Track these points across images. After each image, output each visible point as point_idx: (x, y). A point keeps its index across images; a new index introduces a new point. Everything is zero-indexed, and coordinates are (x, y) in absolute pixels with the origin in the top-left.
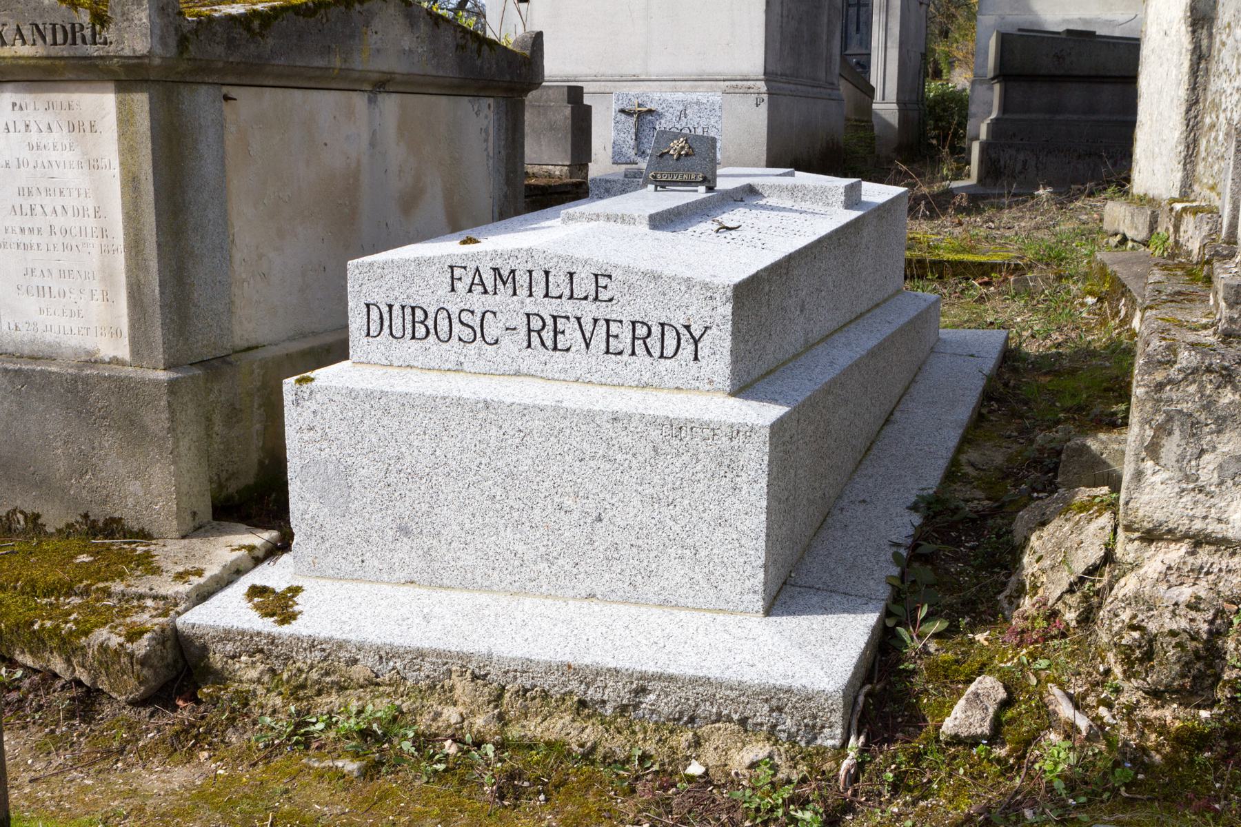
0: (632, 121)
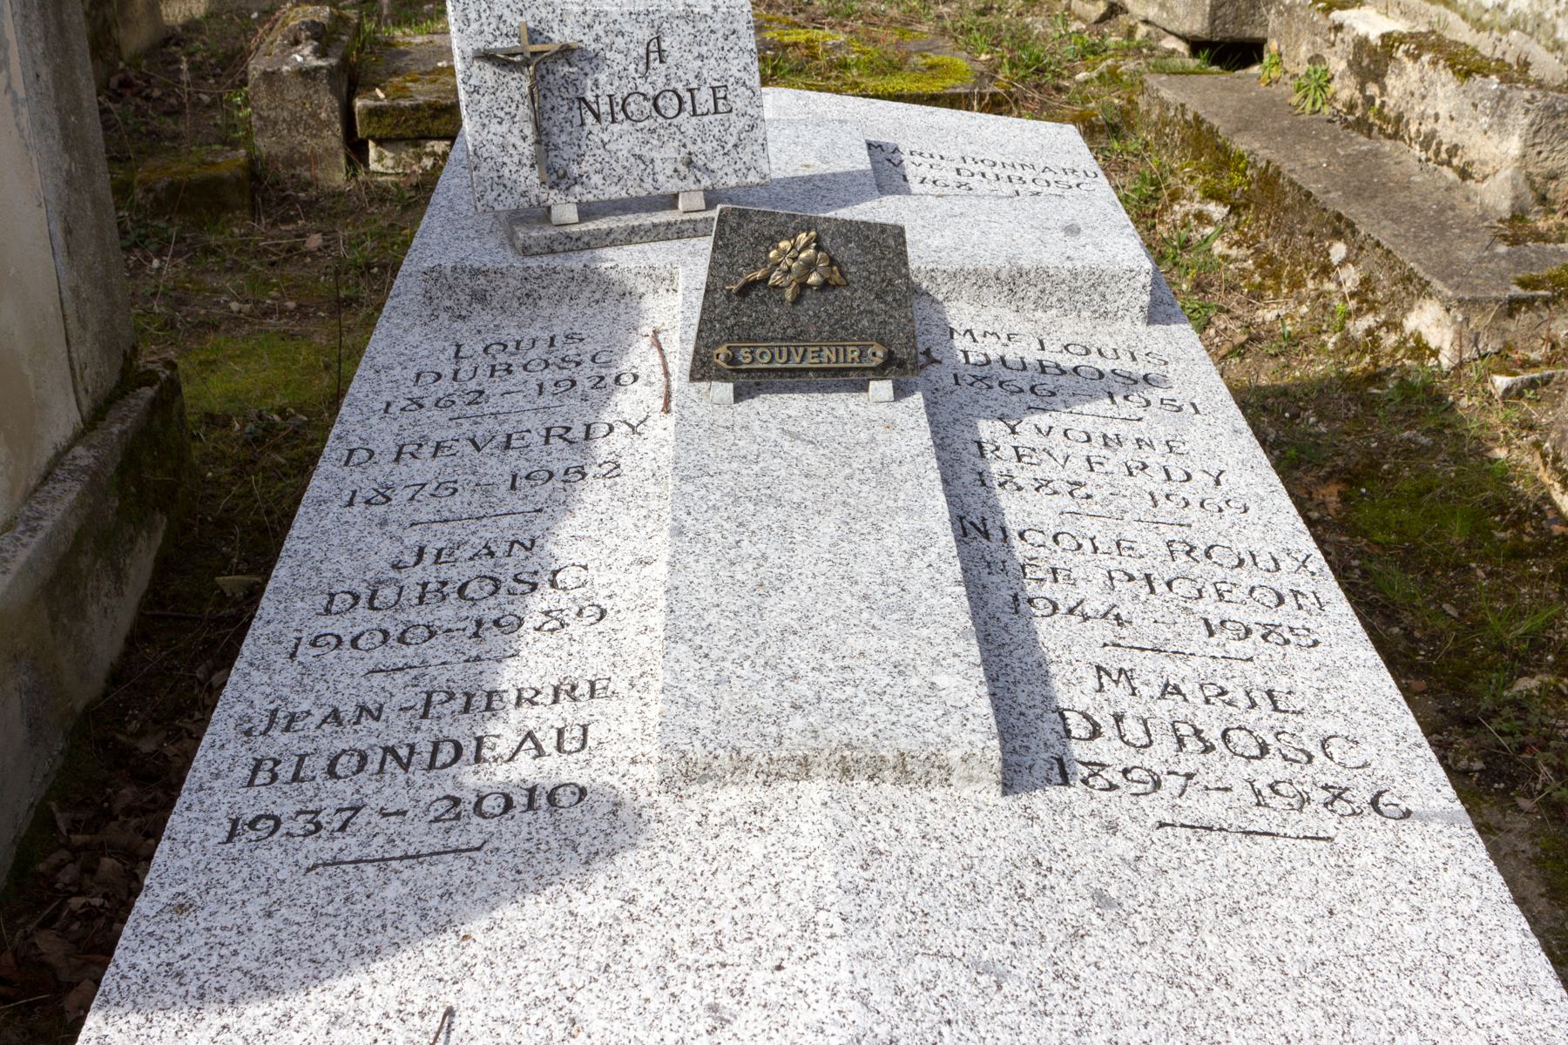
0: (518, 84)
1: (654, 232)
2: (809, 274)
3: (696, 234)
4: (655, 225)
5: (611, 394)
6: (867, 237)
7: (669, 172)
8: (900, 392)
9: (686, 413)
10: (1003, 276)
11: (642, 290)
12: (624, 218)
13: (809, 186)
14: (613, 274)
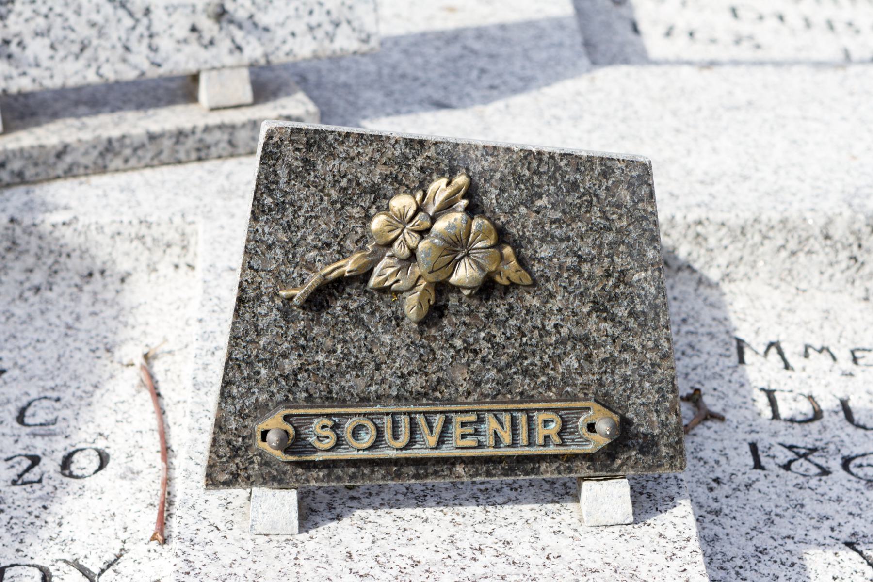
1: (151, 151)
2: (453, 265)
3: (233, 150)
4: (152, 137)
5: (50, 497)
6: (574, 186)
7: (181, 31)
8: (646, 502)
9: (198, 556)
10: (838, 231)
11: (124, 265)
12: (92, 121)
13: (455, 49)
14: (68, 236)
